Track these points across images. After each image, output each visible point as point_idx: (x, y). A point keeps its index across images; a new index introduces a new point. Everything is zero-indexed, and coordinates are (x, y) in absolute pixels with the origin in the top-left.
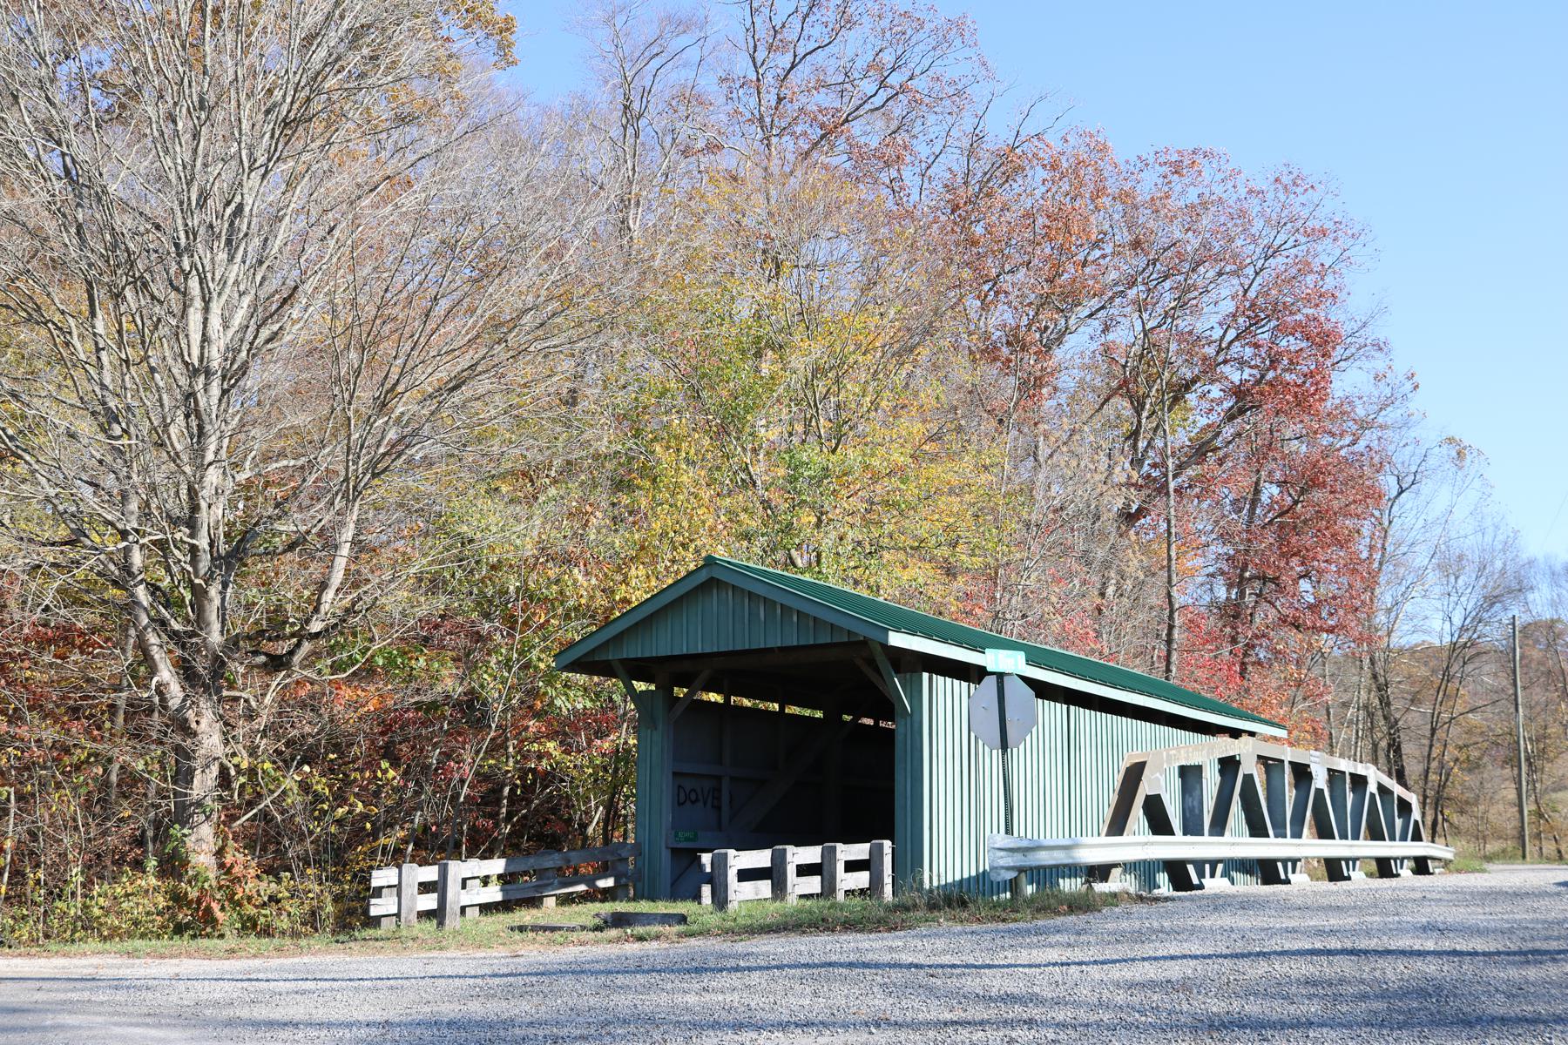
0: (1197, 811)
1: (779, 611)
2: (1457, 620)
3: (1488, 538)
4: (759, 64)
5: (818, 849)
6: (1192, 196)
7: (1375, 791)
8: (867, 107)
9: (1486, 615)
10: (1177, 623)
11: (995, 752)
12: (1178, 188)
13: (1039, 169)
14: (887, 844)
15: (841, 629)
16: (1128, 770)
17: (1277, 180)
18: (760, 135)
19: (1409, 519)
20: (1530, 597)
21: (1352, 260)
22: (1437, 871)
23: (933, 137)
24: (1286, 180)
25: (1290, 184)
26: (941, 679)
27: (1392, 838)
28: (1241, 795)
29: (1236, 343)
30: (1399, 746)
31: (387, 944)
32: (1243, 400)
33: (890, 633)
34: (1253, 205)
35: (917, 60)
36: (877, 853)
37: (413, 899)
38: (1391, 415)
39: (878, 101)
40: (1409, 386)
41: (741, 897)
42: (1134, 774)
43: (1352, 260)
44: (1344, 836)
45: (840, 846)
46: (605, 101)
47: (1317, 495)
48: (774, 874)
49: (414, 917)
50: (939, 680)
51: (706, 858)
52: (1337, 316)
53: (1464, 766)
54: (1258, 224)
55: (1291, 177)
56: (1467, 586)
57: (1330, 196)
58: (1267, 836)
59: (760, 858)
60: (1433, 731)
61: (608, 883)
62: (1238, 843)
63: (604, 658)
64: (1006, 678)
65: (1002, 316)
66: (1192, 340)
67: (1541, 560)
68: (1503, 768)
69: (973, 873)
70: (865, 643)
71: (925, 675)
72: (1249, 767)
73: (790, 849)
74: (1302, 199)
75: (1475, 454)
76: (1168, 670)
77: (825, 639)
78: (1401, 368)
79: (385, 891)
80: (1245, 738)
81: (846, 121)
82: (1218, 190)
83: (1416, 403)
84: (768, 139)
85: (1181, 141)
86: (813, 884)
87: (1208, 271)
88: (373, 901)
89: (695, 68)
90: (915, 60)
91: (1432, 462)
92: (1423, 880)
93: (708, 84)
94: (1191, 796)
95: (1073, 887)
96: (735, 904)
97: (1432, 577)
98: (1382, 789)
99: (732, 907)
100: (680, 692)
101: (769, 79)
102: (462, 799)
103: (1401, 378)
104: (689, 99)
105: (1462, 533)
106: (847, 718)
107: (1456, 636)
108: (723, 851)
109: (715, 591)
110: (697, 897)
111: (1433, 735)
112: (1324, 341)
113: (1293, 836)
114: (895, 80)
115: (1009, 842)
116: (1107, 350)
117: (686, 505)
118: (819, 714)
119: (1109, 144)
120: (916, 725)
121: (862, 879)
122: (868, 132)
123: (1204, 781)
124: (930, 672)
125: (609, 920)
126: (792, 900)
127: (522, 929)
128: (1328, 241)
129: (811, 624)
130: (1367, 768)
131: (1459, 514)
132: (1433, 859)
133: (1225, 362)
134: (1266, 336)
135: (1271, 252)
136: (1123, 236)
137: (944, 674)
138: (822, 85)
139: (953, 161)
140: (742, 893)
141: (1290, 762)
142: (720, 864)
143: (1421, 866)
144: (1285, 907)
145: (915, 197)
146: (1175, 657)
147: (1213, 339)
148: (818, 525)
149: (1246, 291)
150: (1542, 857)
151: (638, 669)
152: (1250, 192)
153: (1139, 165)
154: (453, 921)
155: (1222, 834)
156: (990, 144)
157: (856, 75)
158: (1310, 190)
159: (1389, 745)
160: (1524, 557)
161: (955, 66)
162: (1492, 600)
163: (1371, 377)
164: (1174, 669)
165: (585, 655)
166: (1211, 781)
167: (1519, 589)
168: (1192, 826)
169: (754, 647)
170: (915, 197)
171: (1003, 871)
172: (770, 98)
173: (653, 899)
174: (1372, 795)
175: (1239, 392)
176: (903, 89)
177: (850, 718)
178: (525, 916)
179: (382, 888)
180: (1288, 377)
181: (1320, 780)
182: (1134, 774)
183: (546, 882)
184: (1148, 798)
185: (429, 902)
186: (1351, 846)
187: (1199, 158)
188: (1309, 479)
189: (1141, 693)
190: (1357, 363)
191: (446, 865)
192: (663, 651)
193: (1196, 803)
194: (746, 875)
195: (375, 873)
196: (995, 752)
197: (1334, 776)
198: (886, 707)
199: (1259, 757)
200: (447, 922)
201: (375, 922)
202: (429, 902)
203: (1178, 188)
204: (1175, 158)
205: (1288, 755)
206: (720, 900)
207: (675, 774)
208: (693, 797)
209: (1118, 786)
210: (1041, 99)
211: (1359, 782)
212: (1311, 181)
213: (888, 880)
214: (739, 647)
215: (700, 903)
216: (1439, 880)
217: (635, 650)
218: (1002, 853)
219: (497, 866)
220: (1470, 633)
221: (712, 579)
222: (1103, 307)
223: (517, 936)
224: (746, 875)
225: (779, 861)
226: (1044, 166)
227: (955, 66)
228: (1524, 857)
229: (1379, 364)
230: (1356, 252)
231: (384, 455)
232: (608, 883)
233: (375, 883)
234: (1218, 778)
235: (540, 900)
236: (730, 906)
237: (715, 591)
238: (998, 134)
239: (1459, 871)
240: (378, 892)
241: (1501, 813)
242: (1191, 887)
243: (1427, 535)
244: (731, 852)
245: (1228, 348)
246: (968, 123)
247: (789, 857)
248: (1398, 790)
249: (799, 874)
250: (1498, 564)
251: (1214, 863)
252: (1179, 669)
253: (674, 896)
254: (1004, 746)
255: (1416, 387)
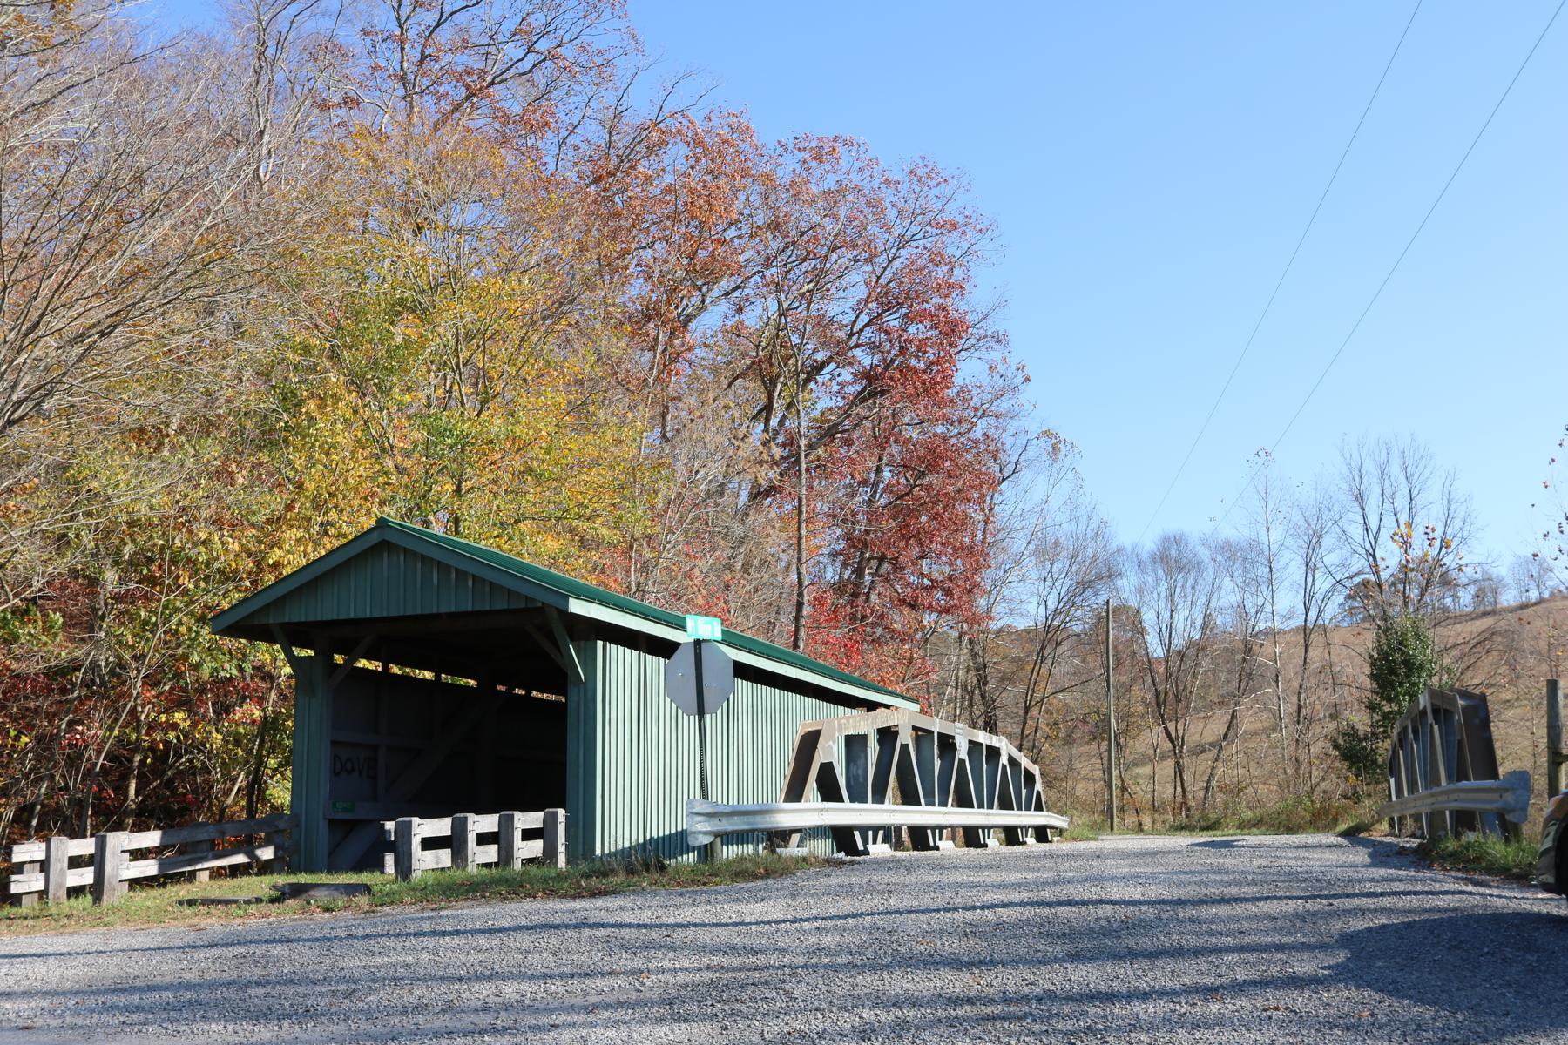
0: (861, 780)
1: (453, 575)
2: (1052, 605)
3: (1082, 527)
4: (403, 20)
5: (495, 818)
6: (831, 183)
7: (1006, 762)
8: (513, 71)
9: (1078, 600)
10: (806, 599)
11: (692, 717)
12: (817, 174)
13: (681, 145)
14: (561, 812)
15: (518, 594)
16: (803, 738)
17: (911, 172)
18: (402, 92)
19: (1008, 509)
20: (1119, 583)
21: (979, 253)
22: (1055, 839)
23: (572, 107)
24: (920, 172)
25: (925, 176)
26: (613, 647)
27: (1020, 808)
28: (818, 781)
29: (868, 329)
30: (996, 724)
31: (39, 922)
32: (873, 384)
33: (571, 599)
34: (888, 197)
35: (567, 26)
36: (551, 821)
37: (63, 875)
38: (1002, 406)
39: (526, 65)
40: (1020, 379)
41: (424, 866)
42: (809, 742)
43: (979, 253)
44: (981, 806)
45: (517, 815)
46: (234, 42)
47: (932, 479)
48: (454, 843)
49: (63, 893)
50: (612, 648)
51: (390, 825)
52: (959, 306)
53: (1055, 742)
54: (891, 214)
55: (926, 170)
56: (1060, 571)
57: (962, 190)
58: (920, 804)
59: (441, 827)
60: (1027, 709)
61: (267, 853)
62: (893, 813)
63: (264, 621)
64: (703, 645)
65: (637, 290)
66: (824, 324)
67: (1130, 549)
68: (1088, 743)
69: (641, 841)
70: (542, 610)
71: (600, 643)
72: (906, 737)
73: (471, 817)
74: (936, 191)
75: (1069, 447)
76: (796, 646)
77: (501, 604)
78: (1013, 361)
79: (26, 867)
80: (880, 710)
81: (492, 83)
82: (855, 177)
83: (1027, 395)
84: (409, 96)
85: (822, 129)
86: (491, 853)
87: (841, 258)
88: (14, 878)
89: (334, 18)
90: (563, 30)
91: (1032, 452)
92: (1044, 847)
93: (348, 36)
94: (855, 764)
95: (746, 851)
96: (419, 873)
97: (1029, 562)
98: (1012, 761)
99: (416, 876)
100: (339, 659)
101: (412, 34)
102: (98, 769)
103: (1013, 368)
104: (328, 51)
105: (1058, 520)
106: (503, 688)
107: (1050, 618)
108: (407, 819)
109: (385, 555)
110: (380, 866)
111: (1026, 713)
112: (951, 330)
113: (940, 805)
114: (543, 45)
115: (704, 807)
116: (737, 330)
117: (341, 466)
118: (472, 683)
119: (752, 126)
120: (589, 694)
121: (535, 848)
122: (512, 99)
123: (869, 750)
124: (604, 640)
125: (287, 890)
126: (472, 869)
127: (190, 903)
128: (955, 234)
129: (487, 589)
130: (1000, 741)
131: (1054, 503)
132: (1051, 827)
133: (857, 346)
134: (896, 323)
135: (903, 242)
136: (761, 218)
137: (616, 643)
138: (466, 45)
139: (593, 133)
140: (426, 862)
141: (939, 733)
142: (405, 832)
143: (1041, 833)
144: (939, 867)
145: (551, 167)
146: (802, 633)
147: (844, 322)
148: (458, 491)
149: (879, 278)
150: (1127, 830)
151: (291, 636)
152: (887, 182)
153: (779, 150)
154: (116, 894)
155: (882, 801)
156: (631, 120)
157: (501, 38)
158: (943, 185)
159: (985, 722)
160: (1114, 545)
161: (602, 37)
162: (1084, 585)
163: (987, 366)
164: (802, 645)
165: (244, 618)
166: (873, 749)
167: (1109, 574)
168: (858, 796)
169: (426, 612)
170: (551, 167)
171: (701, 836)
172: (413, 54)
173: (313, 872)
174: (1004, 766)
175: (869, 376)
176: (552, 56)
177: (517, 691)
178: (183, 891)
179: (23, 863)
180: (913, 362)
181: (962, 753)
182: (809, 742)
183: (200, 855)
184: (902, 746)
185: (86, 876)
186: (988, 815)
187: (839, 146)
188: (930, 458)
189: (794, 665)
190: (977, 354)
191: (105, 837)
192: (329, 615)
193: (860, 772)
194: (428, 844)
195: (16, 848)
196: (692, 717)
197: (974, 746)
198: (560, 678)
199: (914, 728)
200: (105, 897)
201: (16, 900)
202: (86, 876)
203: (817, 174)
204: (814, 144)
205: (937, 725)
206: (404, 868)
207: (334, 743)
208: (349, 767)
209: (796, 747)
210: (685, 76)
211: (994, 753)
212: (945, 175)
213: (561, 849)
214: (393, 613)
215: (383, 872)
216: (1057, 845)
217: (297, 614)
218: (700, 818)
219: (152, 838)
220: (1062, 616)
221: (384, 540)
222: (738, 287)
223: (188, 910)
224: (428, 844)
225: (460, 830)
226: (687, 144)
227: (602, 37)
228: (1112, 829)
229: (996, 355)
230: (984, 246)
231: (20, 402)
232: (267, 853)
233: (16, 859)
234: (878, 748)
235: (193, 874)
236: (414, 875)
237: (385, 555)
238: (641, 107)
239: (1075, 839)
240: (19, 868)
241: (1086, 788)
242: (859, 853)
243: (1024, 523)
244: (416, 820)
245: (862, 330)
246: (610, 98)
247: (470, 826)
248: (1025, 762)
249: (479, 843)
250: (1090, 551)
251: (876, 829)
252: (806, 645)
253: (358, 868)
254: (701, 712)
255: (1027, 380)
